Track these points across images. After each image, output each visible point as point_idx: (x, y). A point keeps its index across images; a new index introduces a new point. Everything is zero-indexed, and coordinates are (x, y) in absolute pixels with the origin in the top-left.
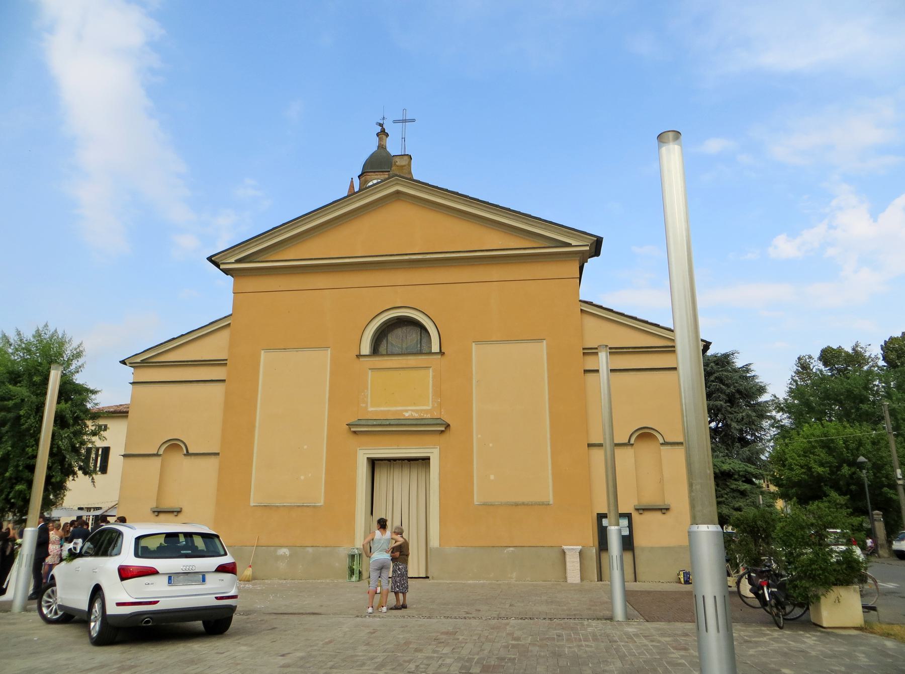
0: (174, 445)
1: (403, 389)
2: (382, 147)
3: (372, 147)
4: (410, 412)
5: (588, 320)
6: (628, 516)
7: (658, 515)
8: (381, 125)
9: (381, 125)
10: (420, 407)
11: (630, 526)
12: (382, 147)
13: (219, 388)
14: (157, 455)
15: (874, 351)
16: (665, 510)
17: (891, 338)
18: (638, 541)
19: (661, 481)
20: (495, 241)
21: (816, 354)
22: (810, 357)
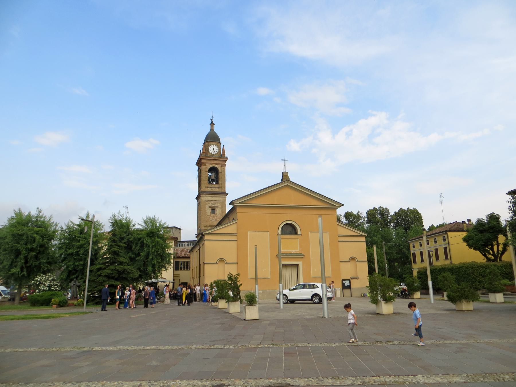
0: (222, 260)
1: (291, 245)
2: (212, 130)
3: (208, 130)
4: (293, 251)
5: (339, 227)
6: (350, 280)
7: (356, 280)
8: (212, 120)
9: (212, 120)
10: (295, 250)
11: (350, 283)
12: (212, 130)
13: (235, 243)
14: (216, 263)
15: (364, 215)
16: (357, 278)
17: (370, 210)
18: (352, 286)
19: (356, 270)
20: (314, 203)
21: (343, 214)
22: (341, 215)
